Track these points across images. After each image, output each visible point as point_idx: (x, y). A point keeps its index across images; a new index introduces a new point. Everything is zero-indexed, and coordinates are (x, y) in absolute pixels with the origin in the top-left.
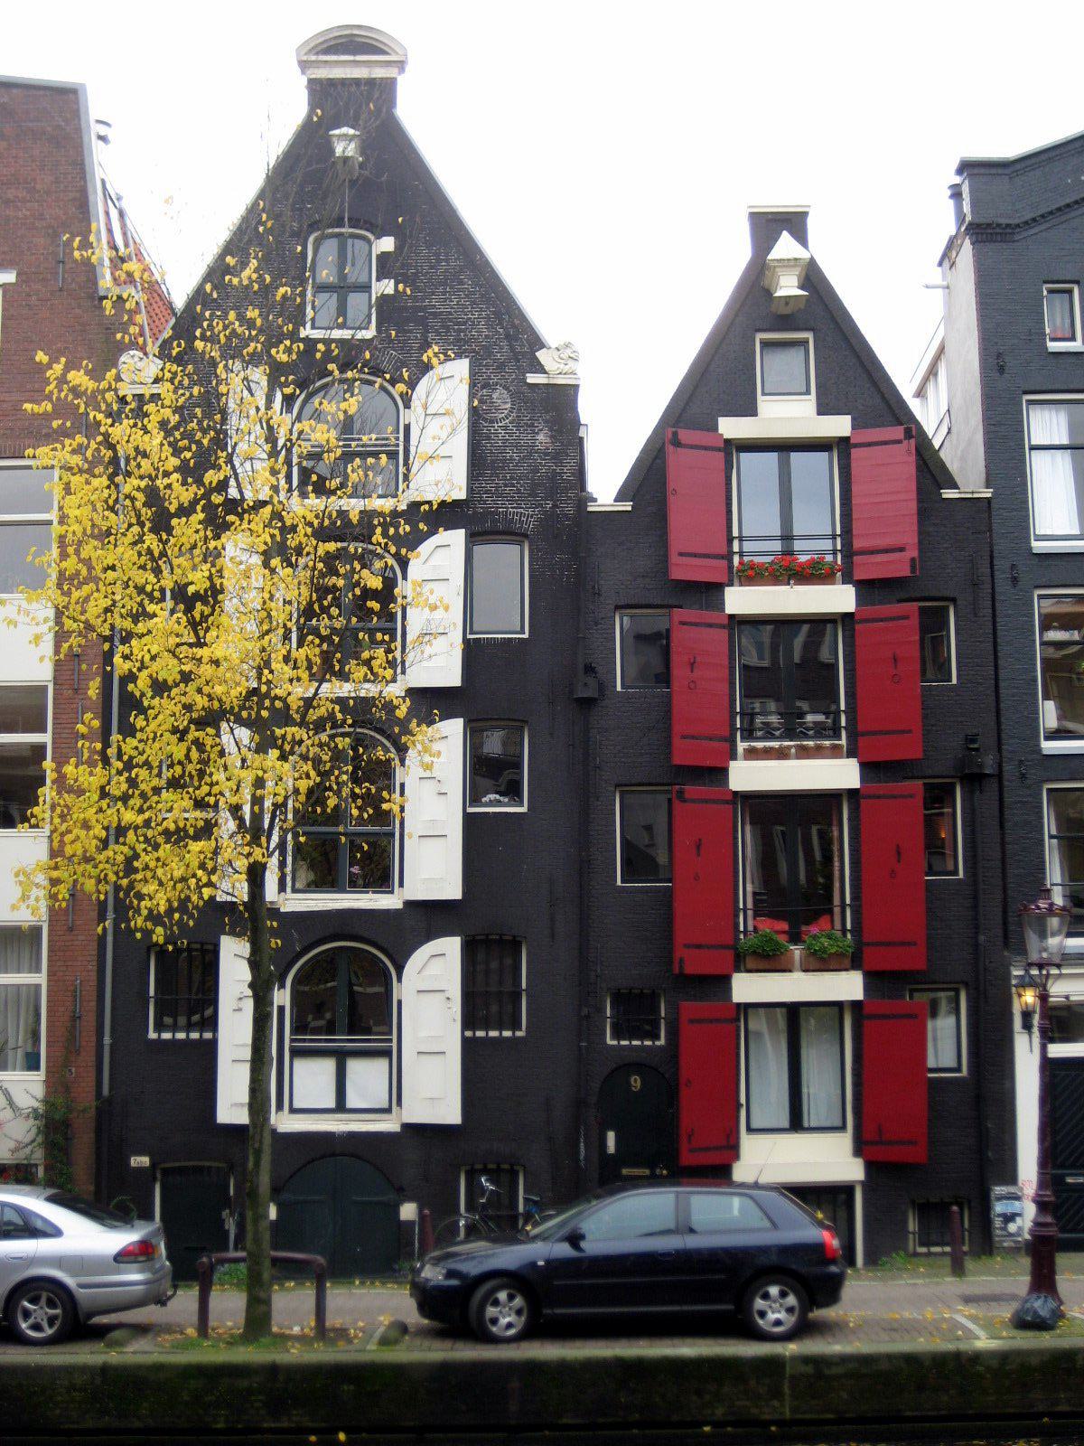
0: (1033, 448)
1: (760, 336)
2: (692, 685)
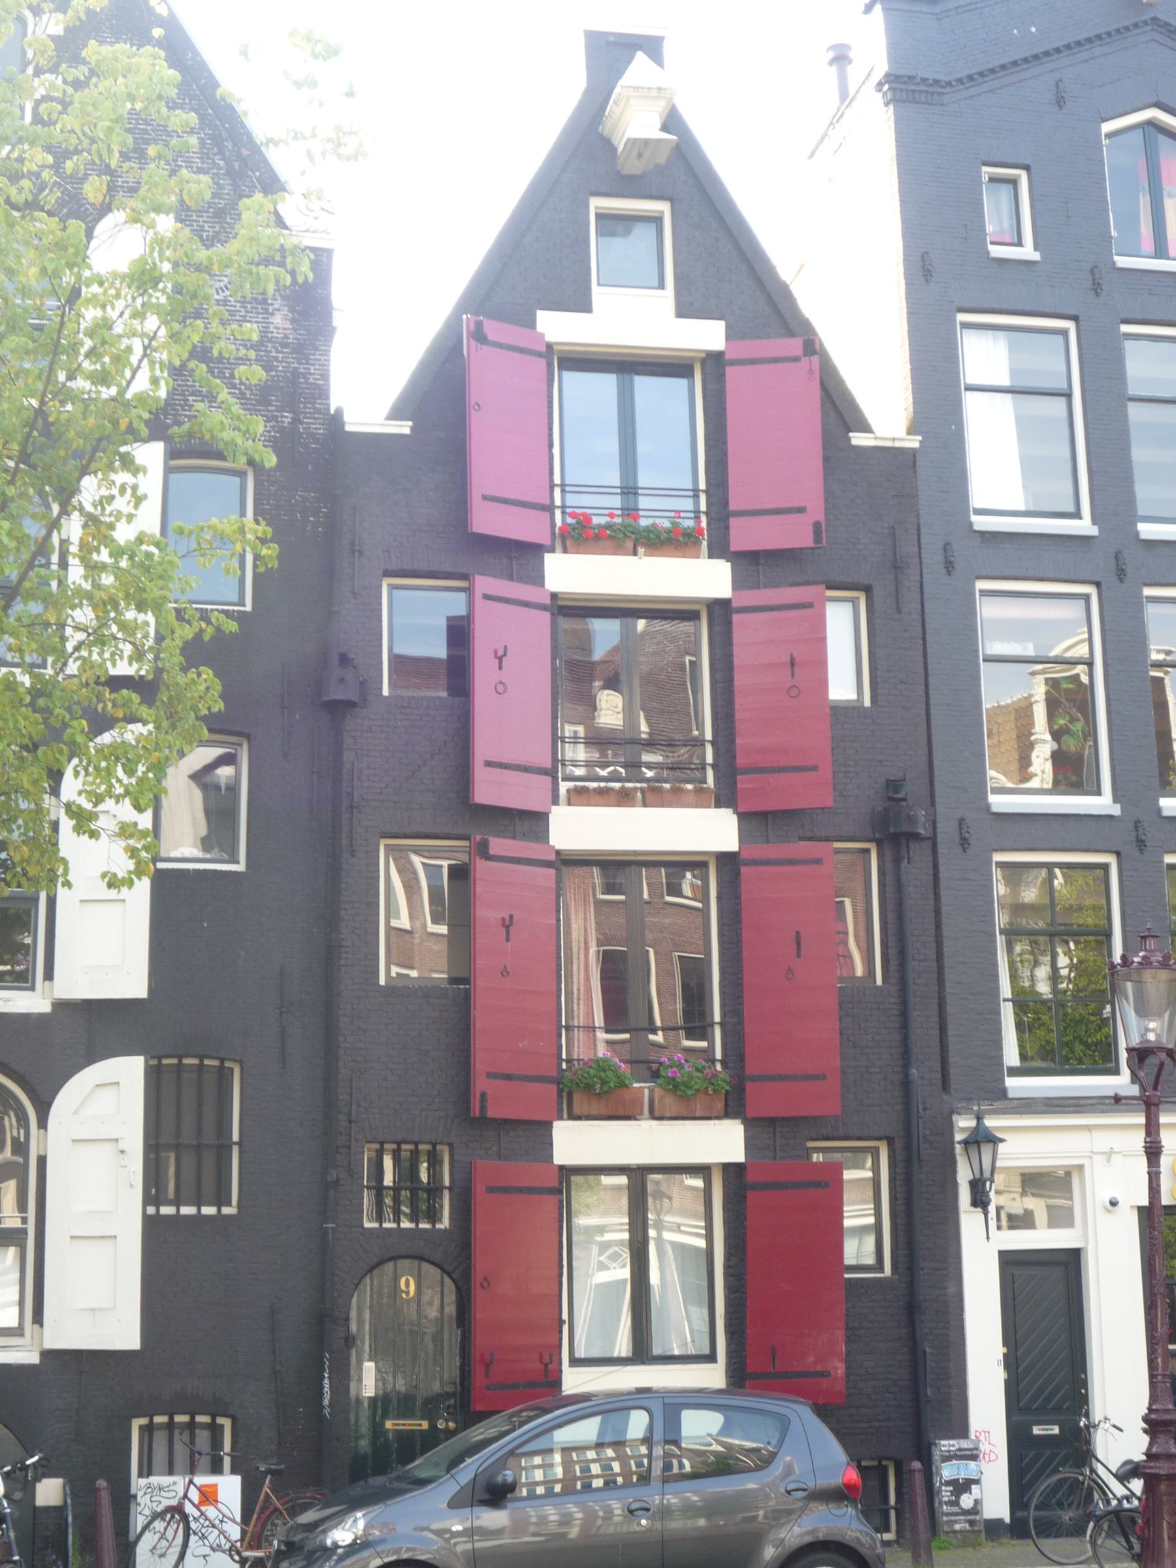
0: (969, 388)
1: (597, 204)
2: (500, 688)
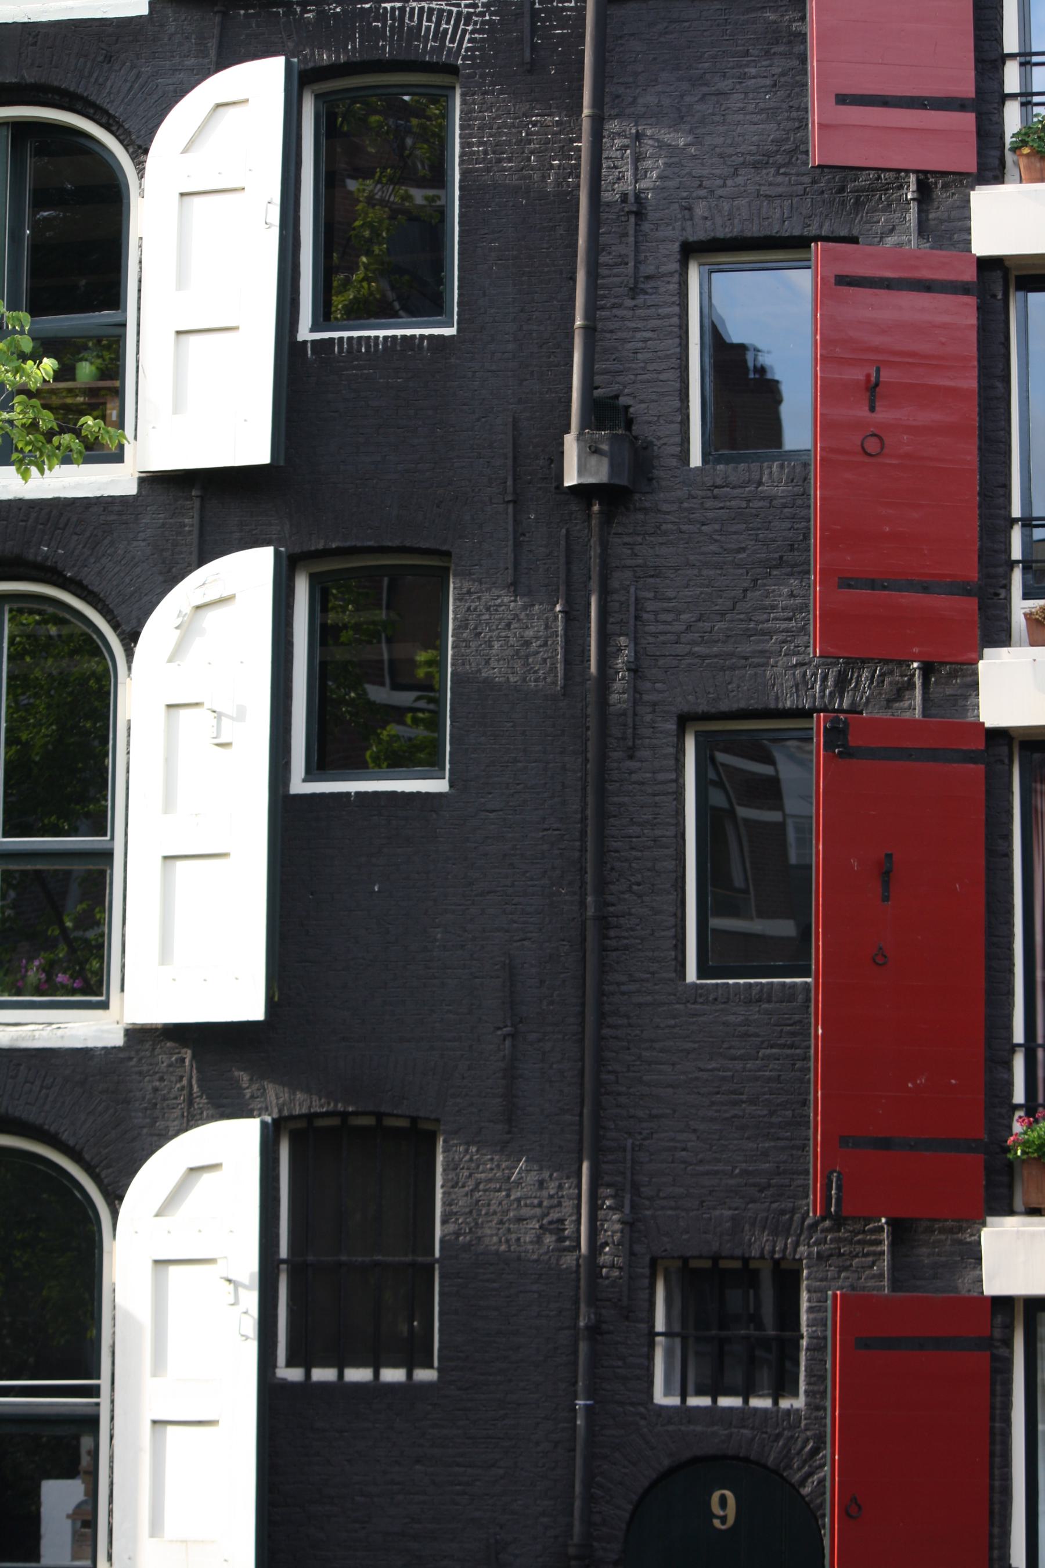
2: (872, 446)
